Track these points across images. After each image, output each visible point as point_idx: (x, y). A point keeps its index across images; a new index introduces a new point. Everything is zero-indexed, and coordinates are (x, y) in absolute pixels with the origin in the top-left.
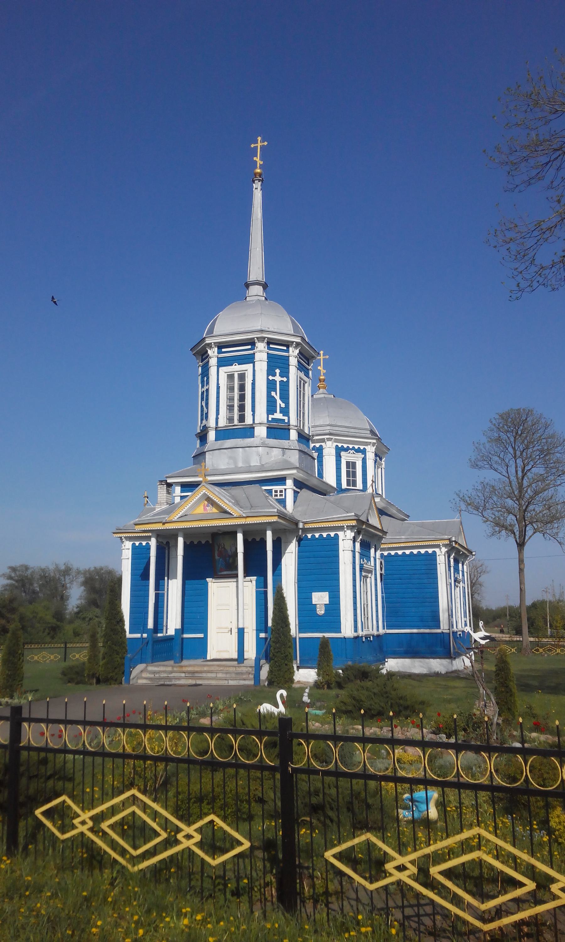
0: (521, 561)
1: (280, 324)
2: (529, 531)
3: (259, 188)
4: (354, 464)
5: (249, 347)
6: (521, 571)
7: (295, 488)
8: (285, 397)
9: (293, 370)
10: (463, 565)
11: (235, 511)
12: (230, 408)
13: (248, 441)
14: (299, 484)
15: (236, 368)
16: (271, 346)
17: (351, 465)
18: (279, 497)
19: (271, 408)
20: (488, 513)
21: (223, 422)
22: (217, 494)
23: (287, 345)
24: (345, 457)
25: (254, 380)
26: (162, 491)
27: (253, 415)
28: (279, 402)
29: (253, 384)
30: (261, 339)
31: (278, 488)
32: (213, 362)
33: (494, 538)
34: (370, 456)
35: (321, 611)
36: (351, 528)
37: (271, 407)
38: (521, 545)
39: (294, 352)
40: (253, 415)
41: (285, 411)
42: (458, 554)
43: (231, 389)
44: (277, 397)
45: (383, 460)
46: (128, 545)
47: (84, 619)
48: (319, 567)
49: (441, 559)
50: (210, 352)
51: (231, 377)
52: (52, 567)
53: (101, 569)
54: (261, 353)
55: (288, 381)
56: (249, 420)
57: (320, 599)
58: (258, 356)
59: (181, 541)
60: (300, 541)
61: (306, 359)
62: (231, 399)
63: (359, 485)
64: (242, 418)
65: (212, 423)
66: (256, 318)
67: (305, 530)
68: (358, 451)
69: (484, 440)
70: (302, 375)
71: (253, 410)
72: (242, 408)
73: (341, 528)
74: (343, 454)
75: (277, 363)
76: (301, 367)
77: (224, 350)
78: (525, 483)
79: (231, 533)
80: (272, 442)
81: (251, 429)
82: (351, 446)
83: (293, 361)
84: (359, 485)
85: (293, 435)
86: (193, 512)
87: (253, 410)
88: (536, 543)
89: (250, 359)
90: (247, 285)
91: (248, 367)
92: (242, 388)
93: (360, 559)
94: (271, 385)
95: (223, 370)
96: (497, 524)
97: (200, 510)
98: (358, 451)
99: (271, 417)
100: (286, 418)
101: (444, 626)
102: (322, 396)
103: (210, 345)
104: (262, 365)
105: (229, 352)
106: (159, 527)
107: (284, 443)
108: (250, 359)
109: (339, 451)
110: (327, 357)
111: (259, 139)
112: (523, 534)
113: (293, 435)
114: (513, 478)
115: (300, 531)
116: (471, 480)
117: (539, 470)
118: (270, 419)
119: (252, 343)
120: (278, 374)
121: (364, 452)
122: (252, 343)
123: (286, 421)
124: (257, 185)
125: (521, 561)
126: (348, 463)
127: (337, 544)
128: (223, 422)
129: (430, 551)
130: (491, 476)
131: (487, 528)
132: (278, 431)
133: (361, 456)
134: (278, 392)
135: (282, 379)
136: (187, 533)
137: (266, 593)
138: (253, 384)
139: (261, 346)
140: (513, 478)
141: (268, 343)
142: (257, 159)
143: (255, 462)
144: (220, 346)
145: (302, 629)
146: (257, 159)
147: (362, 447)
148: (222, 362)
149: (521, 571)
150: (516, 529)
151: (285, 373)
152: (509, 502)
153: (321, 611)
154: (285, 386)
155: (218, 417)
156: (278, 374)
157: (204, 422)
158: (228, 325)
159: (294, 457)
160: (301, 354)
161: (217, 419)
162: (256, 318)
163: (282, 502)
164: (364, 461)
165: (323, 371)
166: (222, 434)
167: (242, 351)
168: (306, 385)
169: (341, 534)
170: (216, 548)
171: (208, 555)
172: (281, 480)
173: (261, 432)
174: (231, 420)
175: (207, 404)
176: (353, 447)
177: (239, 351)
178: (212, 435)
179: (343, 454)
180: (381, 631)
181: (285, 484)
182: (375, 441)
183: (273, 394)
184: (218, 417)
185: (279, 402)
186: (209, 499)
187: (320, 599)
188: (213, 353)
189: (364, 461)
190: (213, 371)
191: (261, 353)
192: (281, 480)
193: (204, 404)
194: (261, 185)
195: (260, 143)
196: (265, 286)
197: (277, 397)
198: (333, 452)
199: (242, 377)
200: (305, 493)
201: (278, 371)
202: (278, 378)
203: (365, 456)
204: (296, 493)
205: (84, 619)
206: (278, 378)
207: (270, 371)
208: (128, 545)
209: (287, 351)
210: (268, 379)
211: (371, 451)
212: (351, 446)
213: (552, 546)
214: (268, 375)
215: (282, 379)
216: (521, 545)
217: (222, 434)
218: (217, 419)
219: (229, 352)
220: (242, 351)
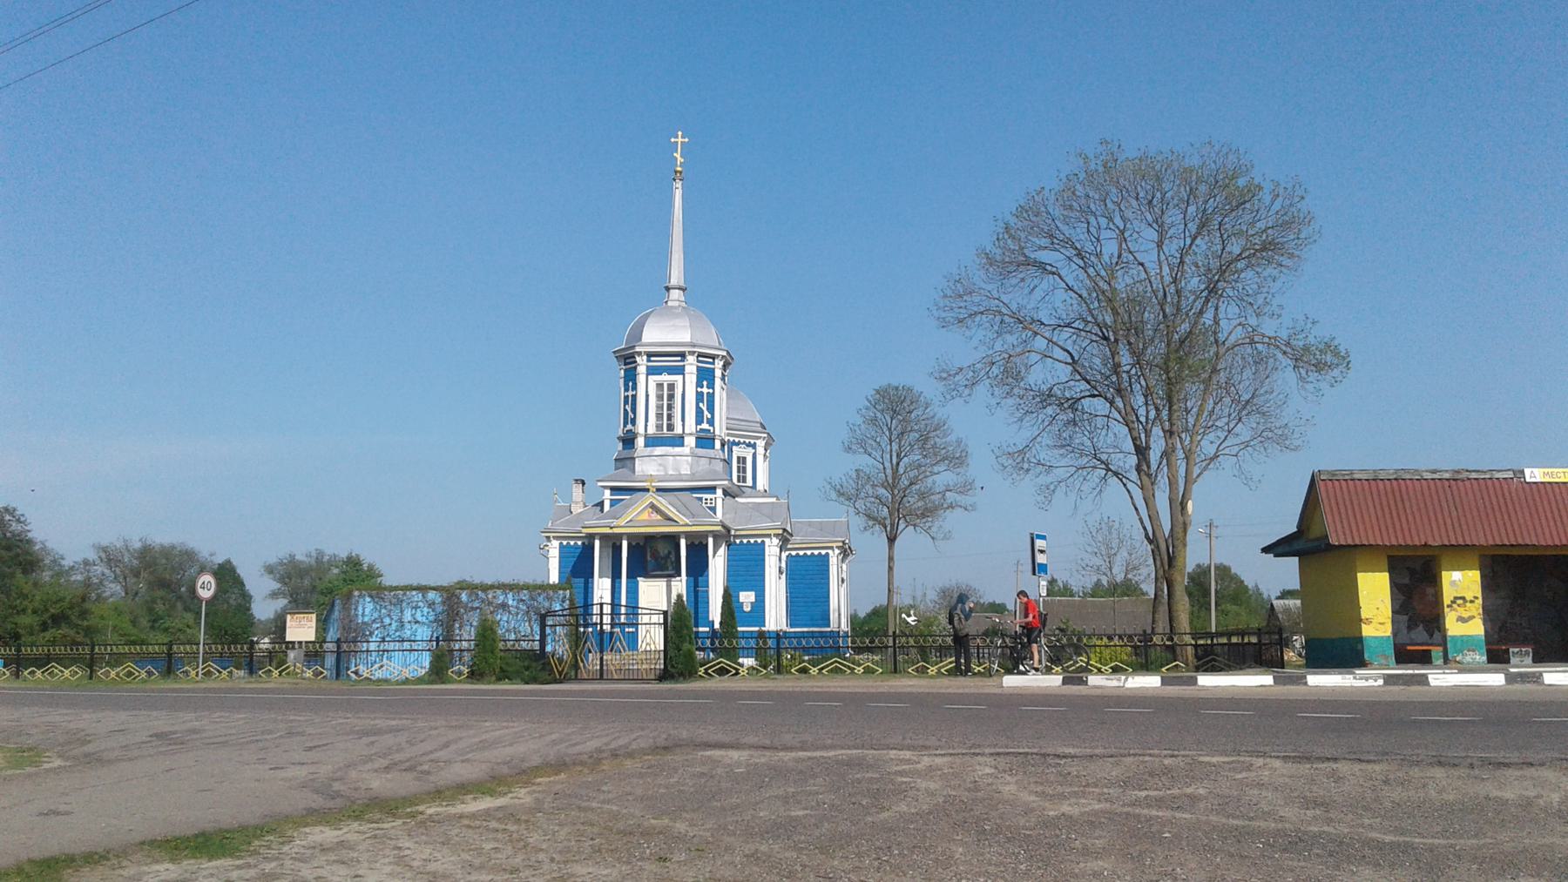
0: (891, 559)
2: (902, 525)
6: (890, 568)
9: (718, 382)
11: (682, 519)
12: (659, 416)
13: (678, 450)
14: (726, 493)
15: (666, 378)
19: (699, 421)
20: (860, 504)
21: (652, 430)
22: (662, 502)
23: (713, 357)
26: (577, 491)
30: (692, 353)
32: (642, 370)
33: (868, 533)
34: (760, 450)
35: (747, 608)
36: (776, 535)
38: (892, 540)
39: (719, 364)
41: (711, 422)
42: (846, 552)
43: (660, 397)
46: (556, 543)
47: (166, 630)
48: (747, 568)
49: (833, 560)
50: (638, 359)
51: (660, 386)
52: (119, 545)
53: (173, 547)
54: (691, 365)
56: (678, 430)
57: (747, 598)
58: (688, 369)
59: (625, 544)
62: (660, 407)
63: (749, 482)
64: (671, 427)
65: (640, 429)
68: (749, 445)
69: (859, 421)
72: (670, 417)
73: (769, 536)
75: (705, 376)
78: (901, 470)
79: (673, 539)
80: (701, 451)
81: (681, 437)
83: (718, 373)
84: (749, 482)
85: (718, 444)
86: (637, 518)
88: (907, 536)
89: (680, 371)
90: (668, 289)
92: (671, 397)
94: (699, 396)
96: (869, 517)
97: (645, 516)
98: (749, 445)
101: (833, 626)
103: (639, 354)
104: (691, 378)
105: (658, 362)
106: (607, 530)
107: (710, 452)
108: (680, 371)
112: (895, 527)
113: (718, 444)
114: (887, 465)
116: (845, 466)
117: (916, 456)
119: (683, 355)
121: (754, 446)
122: (683, 355)
124: (679, 184)
125: (891, 559)
128: (652, 430)
130: (864, 462)
131: (860, 521)
136: (630, 537)
139: (691, 359)
140: (887, 465)
142: (678, 155)
143: (685, 470)
144: (650, 355)
146: (678, 155)
148: (651, 371)
149: (890, 568)
150: (888, 522)
151: (711, 385)
152: (882, 491)
153: (747, 608)
154: (711, 396)
155: (646, 424)
157: (629, 427)
164: (754, 456)
166: (651, 441)
169: (767, 540)
171: (651, 554)
172: (712, 489)
173: (690, 441)
174: (659, 427)
175: (634, 410)
178: (640, 441)
180: (785, 628)
186: (653, 506)
188: (642, 362)
189: (754, 456)
190: (641, 379)
191: (691, 365)
192: (712, 489)
193: (628, 408)
199: (671, 387)
202: (705, 390)
205: (166, 630)
206: (705, 390)
207: (699, 384)
208: (556, 543)
211: (761, 444)
213: (923, 539)
216: (892, 540)
217: (651, 441)
219: (658, 362)
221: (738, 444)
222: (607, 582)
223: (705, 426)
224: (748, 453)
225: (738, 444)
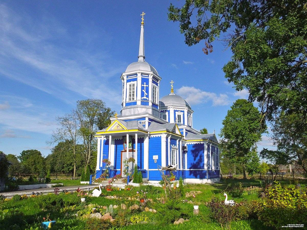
1: (146, 69)
3: (143, 27)
4: (180, 116)
5: (136, 76)
7: (149, 121)
8: (147, 91)
10: (179, 141)
11: (125, 128)
15: (132, 83)
16: (143, 75)
17: (179, 116)
18: (143, 124)
21: (128, 100)
24: (177, 113)
25: (137, 86)
27: (137, 97)
28: (145, 93)
29: (137, 87)
31: (143, 121)
37: (142, 95)
40: (137, 97)
41: (147, 96)
44: (145, 92)
45: (192, 114)
51: (130, 85)
54: (139, 77)
55: (148, 87)
56: (135, 99)
58: (138, 79)
60: (149, 138)
61: (155, 80)
63: (167, 121)
66: (142, 68)
67: (150, 135)
68: (182, 111)
70: (155, 85)
71: (137, 96)
74: (176, 112)
75: (145, 81)
76: (153, 82)
77: (128, 77)
82: (179, 110)
84: (182, 123)
87: (137, 96)
89: (136, 80)
91: (135, 82)
93: (170, 145)
94: (142, 88)
95: (129, 83)
98: (182, 111)
99: (142, 98)
100: (148, 98)
102: (172, 94)
103: (124, 76)
105: (130, 78)
108: (136, 80)
109: (175, 111)
110: (174, 82)
111: (143, 13)
113: (150, 104)
115: (149, 135)
118: (142, 99)
119: (136, 74)
120: (145, 84)
121: (183, 112)
123: (148, 99)
126: (178, 115)
127: (161, 139)
129: (159, 135)
132: (144, 103)
133: (182, 113)
134: (145, 90)
135: (147, 86)
137: (182, 161)
138: (137, 87)
139: (139, 75)
141: (142, 74)
145: (150, 167)
147: (183, 110)
148: (128, 81)
151: (147, 83)
154: (147, 88)
156: (145, 84)
158: (130, 70)
159: (150, 111)
160: (154, 77)
161: (126, 99)
162: (142, 68)
163: (144, 126)
164: (184, 114)
165: (172, 87)
167: (133, 77)
168: (157, 88)
170: (124, 140)
172: (144, 118)
173: (139, 103)
176: (180, 110)
177: (132, 78)
178: (124, 105)
179: (176, 112)
181: (145, 120)
182: (187, 108)
183: (143, 90)
184: (126, 99)
185: (145, 93)
187: (155, 157)
189: (184, 114)
194: (143, 27)
195: (143, 14)
196: (144, 58)
197: (145, 92)
198: (173, 112)
199: (134, 85)
200: (153, 123)
201: (145, 83)
202: (145, 86)
203: (184, 113)
204: (149, 124)
206: (145, 86)
207: (142, 83)
209: (148, 77)
210: (141, 86)
211: (186, 111)
212: (179, 110)
214: (142, 84)
215: (147, 86)
217: (128, 104)
218: (126, 99)
220: (133, 77)
221: (178, 111)
222: (214, 167)
223: (145, 98)
224: (181, 114)
225: (178, 111)
